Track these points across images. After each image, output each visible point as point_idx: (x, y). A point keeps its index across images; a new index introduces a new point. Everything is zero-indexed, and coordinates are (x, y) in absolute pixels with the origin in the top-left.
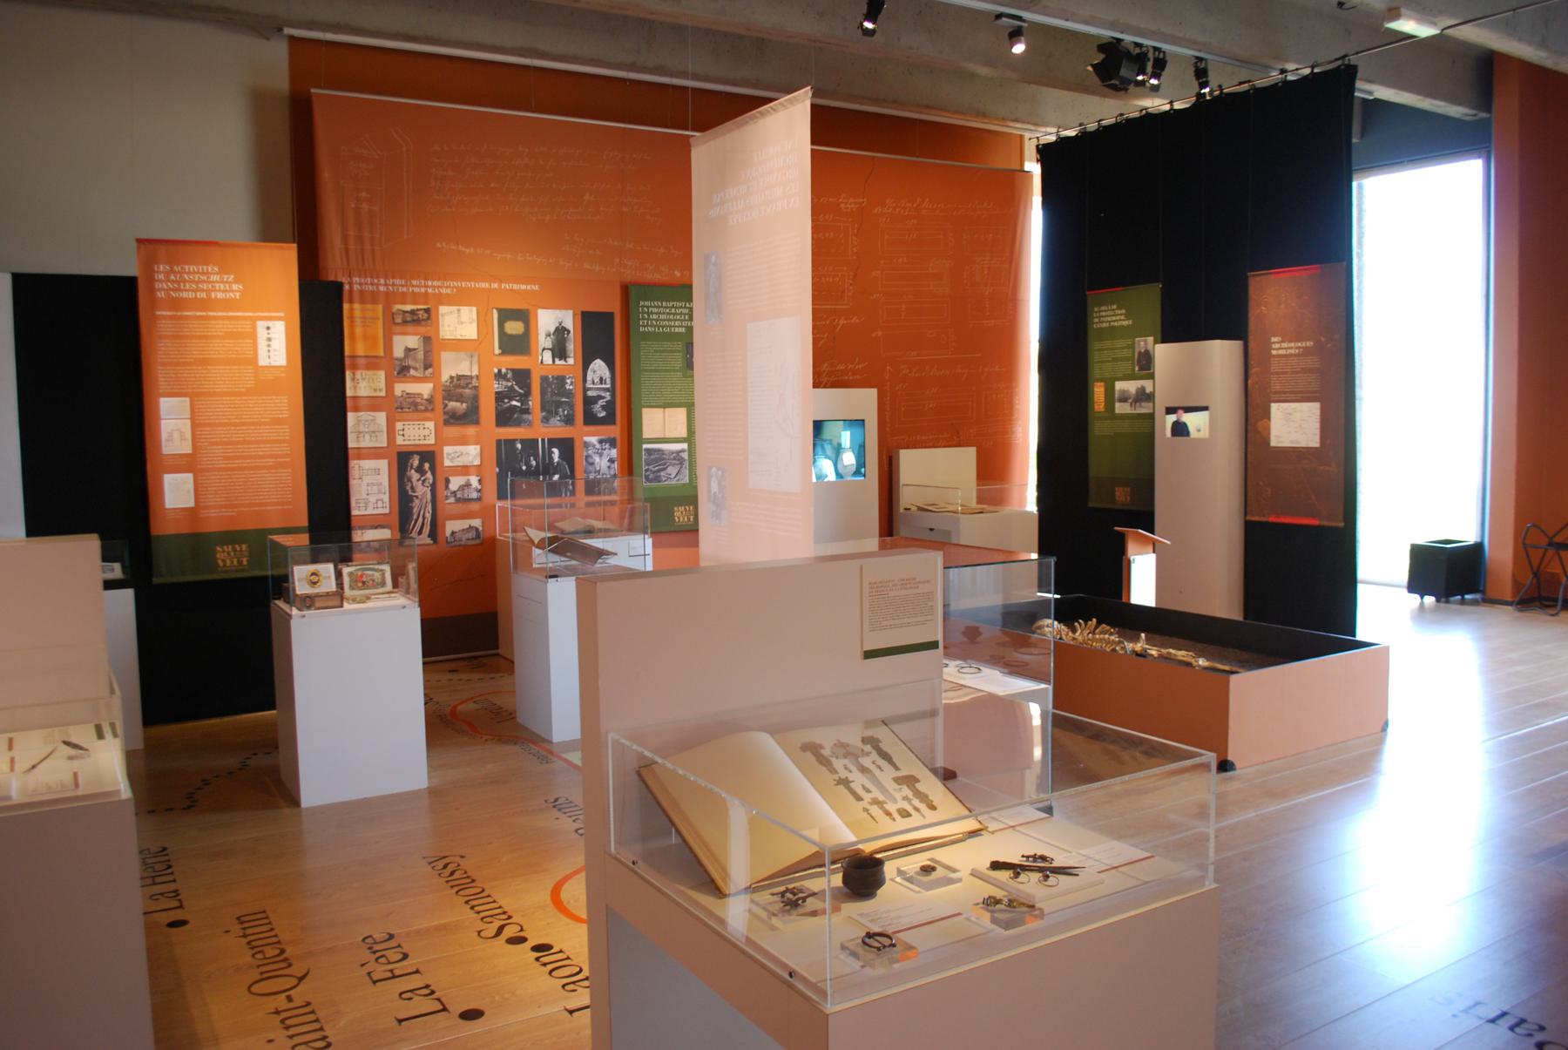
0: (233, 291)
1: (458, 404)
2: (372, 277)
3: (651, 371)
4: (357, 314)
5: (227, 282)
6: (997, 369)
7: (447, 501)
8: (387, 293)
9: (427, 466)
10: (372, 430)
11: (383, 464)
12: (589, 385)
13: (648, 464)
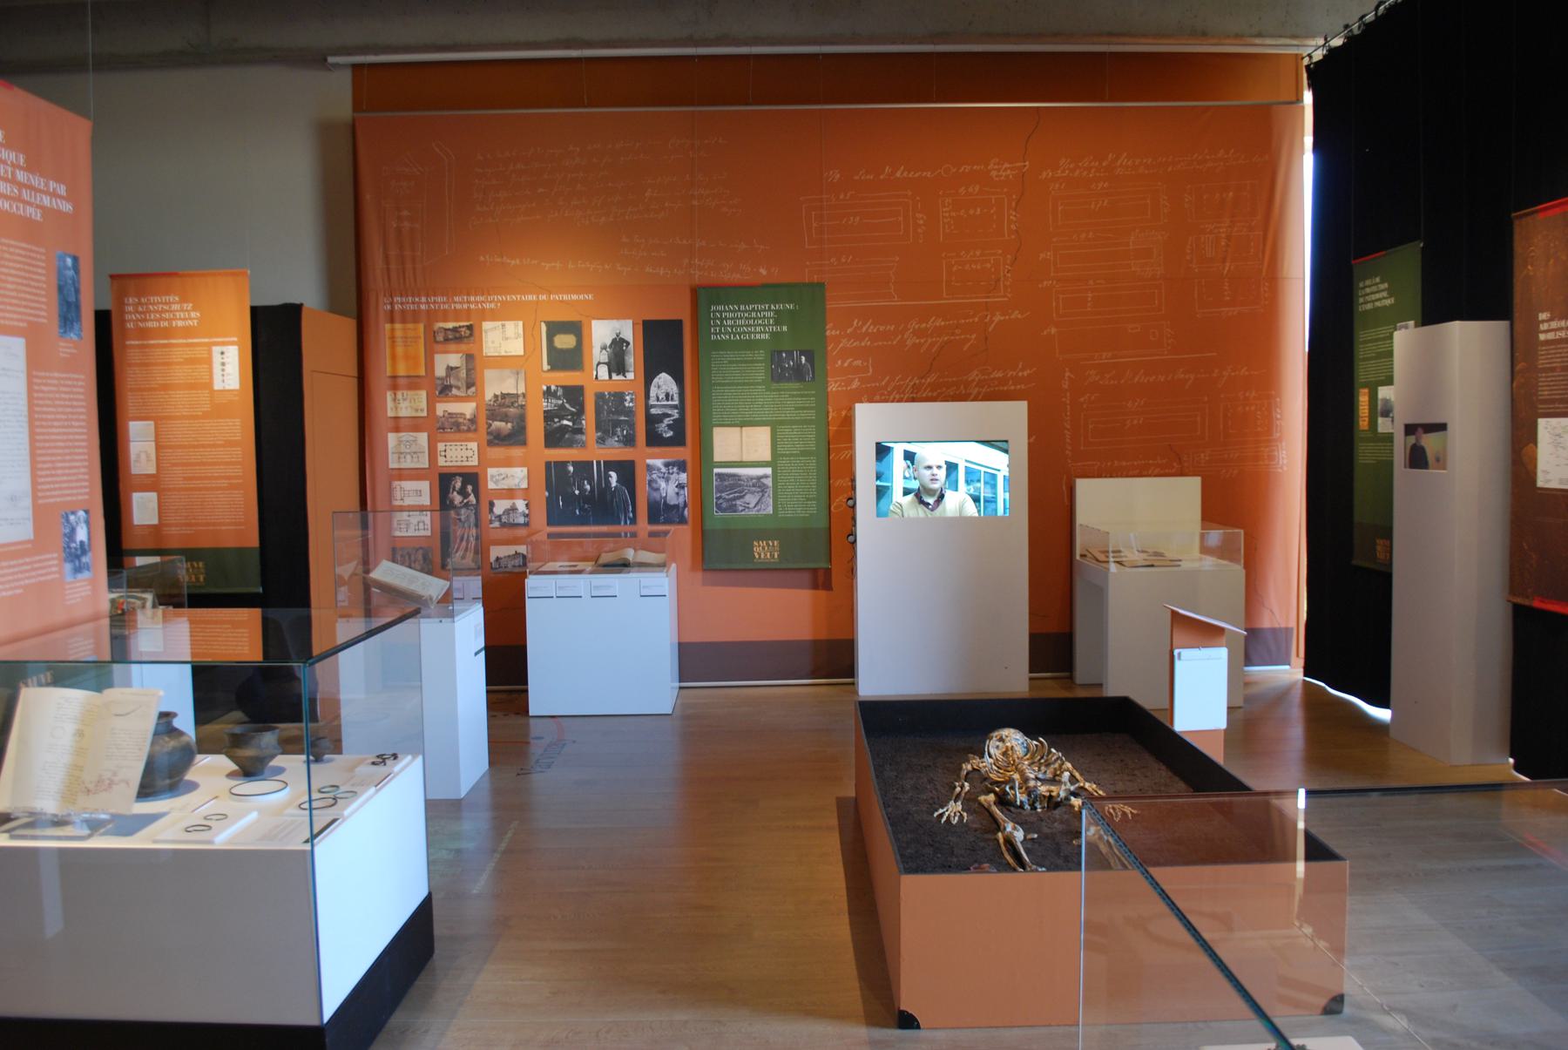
0: (191, 319)
1: (503, 424)
2: (413, 296)
3: (724, 385)
4: (399, 333)
5: (186, 310)
6: (1244, 372)
7: (491, 526)
8: (428, 312)
9: (470, 488)
10: (414, 450)
11: (425, 486)
12: (652, 401)
13: (720, 490)
